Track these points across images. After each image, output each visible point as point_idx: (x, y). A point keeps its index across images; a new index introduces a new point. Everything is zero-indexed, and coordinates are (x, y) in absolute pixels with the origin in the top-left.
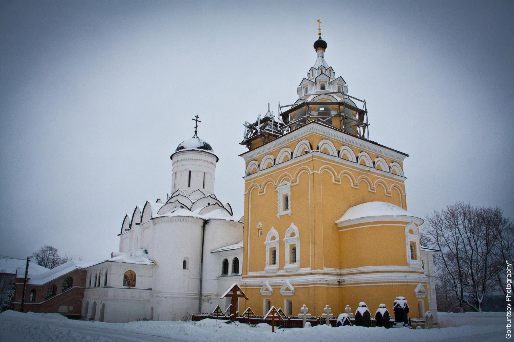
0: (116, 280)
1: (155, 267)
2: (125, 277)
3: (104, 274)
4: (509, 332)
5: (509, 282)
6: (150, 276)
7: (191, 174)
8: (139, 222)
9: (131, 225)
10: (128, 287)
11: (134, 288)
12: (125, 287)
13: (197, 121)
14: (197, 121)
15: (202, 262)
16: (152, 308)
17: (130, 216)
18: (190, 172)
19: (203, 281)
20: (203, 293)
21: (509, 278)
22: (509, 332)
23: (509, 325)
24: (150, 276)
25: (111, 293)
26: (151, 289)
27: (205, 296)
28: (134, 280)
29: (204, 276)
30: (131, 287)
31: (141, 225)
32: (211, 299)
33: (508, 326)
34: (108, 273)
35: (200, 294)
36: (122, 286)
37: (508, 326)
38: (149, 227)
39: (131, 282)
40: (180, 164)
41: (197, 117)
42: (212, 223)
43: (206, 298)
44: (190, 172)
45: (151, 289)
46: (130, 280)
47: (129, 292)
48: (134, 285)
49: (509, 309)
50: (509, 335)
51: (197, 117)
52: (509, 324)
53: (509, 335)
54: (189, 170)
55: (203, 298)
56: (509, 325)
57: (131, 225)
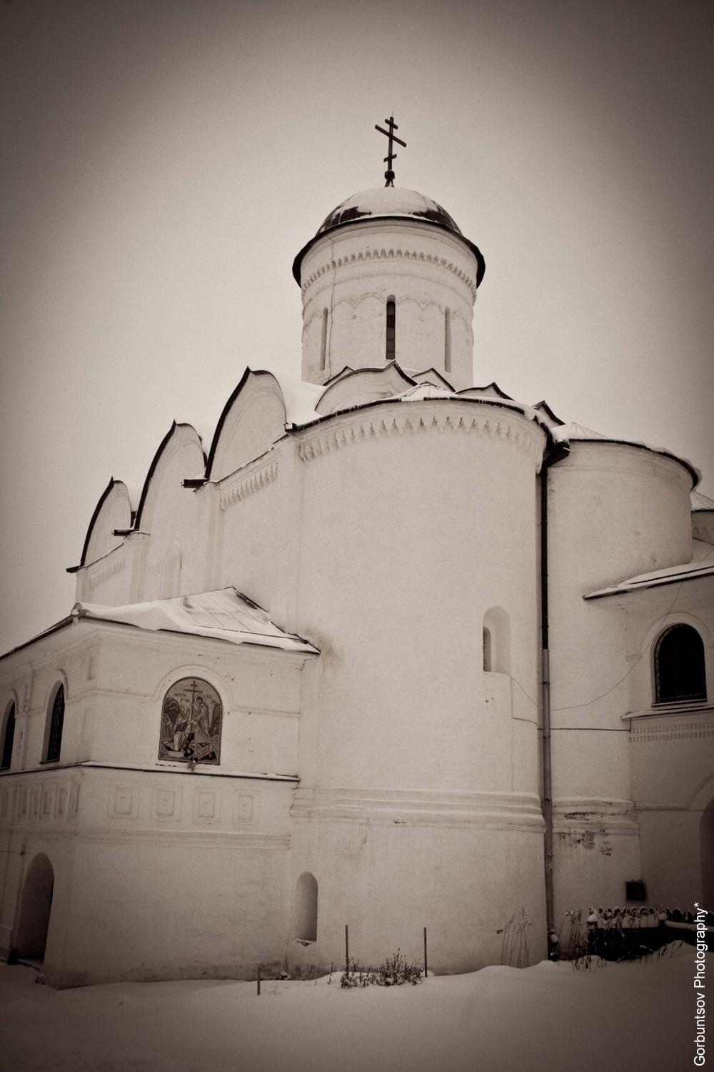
0: (119, 723)
1: (318, 662)
2: (171, 710)
3: (42, 700)
4: (701, 1052)
5: (701, 947)
6: (289, 714)
7: (398, 309)
8: (201, 476)
9: (136, 517)
10: (182, 767)
11: (213, 769)
12: (168, 765)
13: (392, 138)
14: (392, 138)
15: (545, 643)
16: (311, 886)
17: (134, 486)
18: (391, 305)
19: (555, 735)
20: (556, 799)
21: (700, 939)
22: (701, 1052)
23: (701, 1039)
24: (289, 714)
25: (96, 797)
26: (296, 780)
27: (572, 815)
28: (215, 728)
29: (557, 718)
30: (201, 768)
31: (208, 486)
32: (603, 832)
33: (700, 1040)
34: (71, 693)
35: (546, 803)
36: (152, 761)
37: (700, 1040)
38: (270, 478)
39: (199, 739)
40: (343, 272)
41: (390, 122)
42: (579, 456)
43: (577, 828)
44: (391, 305)
45: (296, 780)
46: (192, 729)
47: (186, 791)
48: (213, 758)
49: (701, 1004)
50: (700, 1058)
51: (390, 122)
52: (700, 1035)
53: (700, 1058)
54: (386, 296)
55: (559, 824)
56: (701, 1039)
57: (136, 517)
